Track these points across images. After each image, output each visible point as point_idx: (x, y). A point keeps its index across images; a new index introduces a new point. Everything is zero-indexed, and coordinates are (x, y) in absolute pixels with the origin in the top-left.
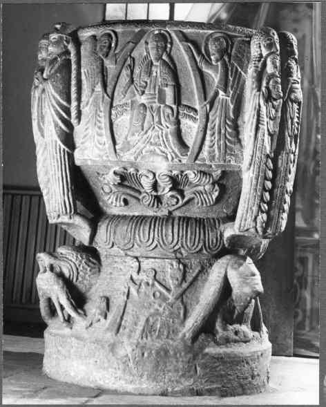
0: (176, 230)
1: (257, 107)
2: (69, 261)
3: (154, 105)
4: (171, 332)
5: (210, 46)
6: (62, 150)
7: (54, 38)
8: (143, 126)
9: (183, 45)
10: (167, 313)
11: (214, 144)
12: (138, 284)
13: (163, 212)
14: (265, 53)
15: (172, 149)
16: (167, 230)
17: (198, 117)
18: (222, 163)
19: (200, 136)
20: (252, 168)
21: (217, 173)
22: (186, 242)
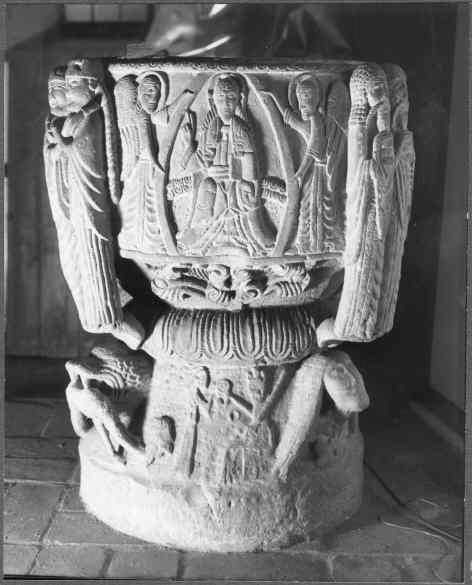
0: (257, 335)
1: (366, 180)
2: (116, 374)
3: (225, 180)
4: (261, 469)
5: (298, 94)
6: (99, 241)
7: (75, 82)
8: (212, 210)
9: (262, 95)
10: (251, 440)
11: (308, 229)
12: (209, 401)
13: (235, 305)
14: (373, 103)
15: (253, 239)
16: (244, 334)
17: (286, 194)
18: (319, 252)
19: (291, 219)
20: (360, 260)
21: (310, 263)
22: (271, 348)
